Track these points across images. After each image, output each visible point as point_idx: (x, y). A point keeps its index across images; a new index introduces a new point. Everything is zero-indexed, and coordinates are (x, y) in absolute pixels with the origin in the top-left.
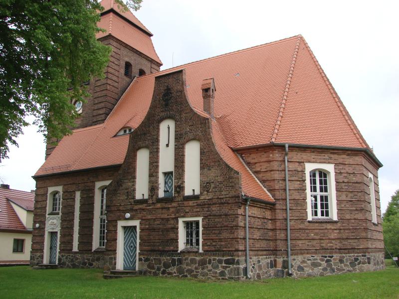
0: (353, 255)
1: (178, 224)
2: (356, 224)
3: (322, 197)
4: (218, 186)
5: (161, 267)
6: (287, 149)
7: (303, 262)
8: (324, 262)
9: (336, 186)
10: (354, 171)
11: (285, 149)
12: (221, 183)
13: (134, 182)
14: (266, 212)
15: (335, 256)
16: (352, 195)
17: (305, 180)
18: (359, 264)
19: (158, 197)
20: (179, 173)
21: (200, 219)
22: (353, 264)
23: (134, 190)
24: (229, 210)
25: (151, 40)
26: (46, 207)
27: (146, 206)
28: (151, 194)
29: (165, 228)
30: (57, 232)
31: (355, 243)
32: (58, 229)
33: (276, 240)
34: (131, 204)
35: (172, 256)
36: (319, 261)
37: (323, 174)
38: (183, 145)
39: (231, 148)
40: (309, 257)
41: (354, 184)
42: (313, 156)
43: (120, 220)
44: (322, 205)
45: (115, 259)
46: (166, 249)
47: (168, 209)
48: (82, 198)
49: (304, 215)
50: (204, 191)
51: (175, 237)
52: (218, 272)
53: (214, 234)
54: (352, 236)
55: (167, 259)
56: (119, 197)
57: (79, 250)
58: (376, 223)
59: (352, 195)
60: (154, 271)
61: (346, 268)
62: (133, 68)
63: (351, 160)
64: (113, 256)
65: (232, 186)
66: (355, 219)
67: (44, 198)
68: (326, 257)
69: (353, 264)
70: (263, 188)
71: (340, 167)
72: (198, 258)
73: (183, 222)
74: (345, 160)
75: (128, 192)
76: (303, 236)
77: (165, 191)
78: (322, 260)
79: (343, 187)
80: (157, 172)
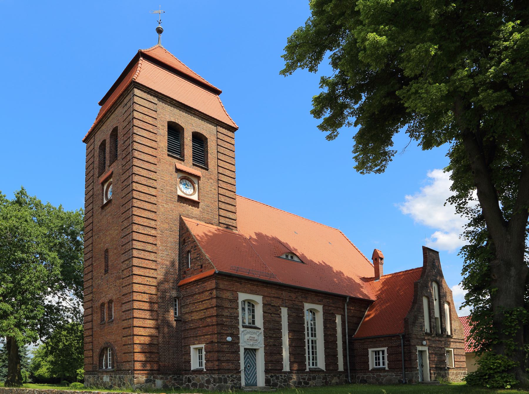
3: (312, 341)
21: (385, 349)
30: (426, 351)
34: (424, 335)
47: (441, 341)
48: (289, 316)
53: (459, 358)
57: (389, 369)
67: (234, 305)
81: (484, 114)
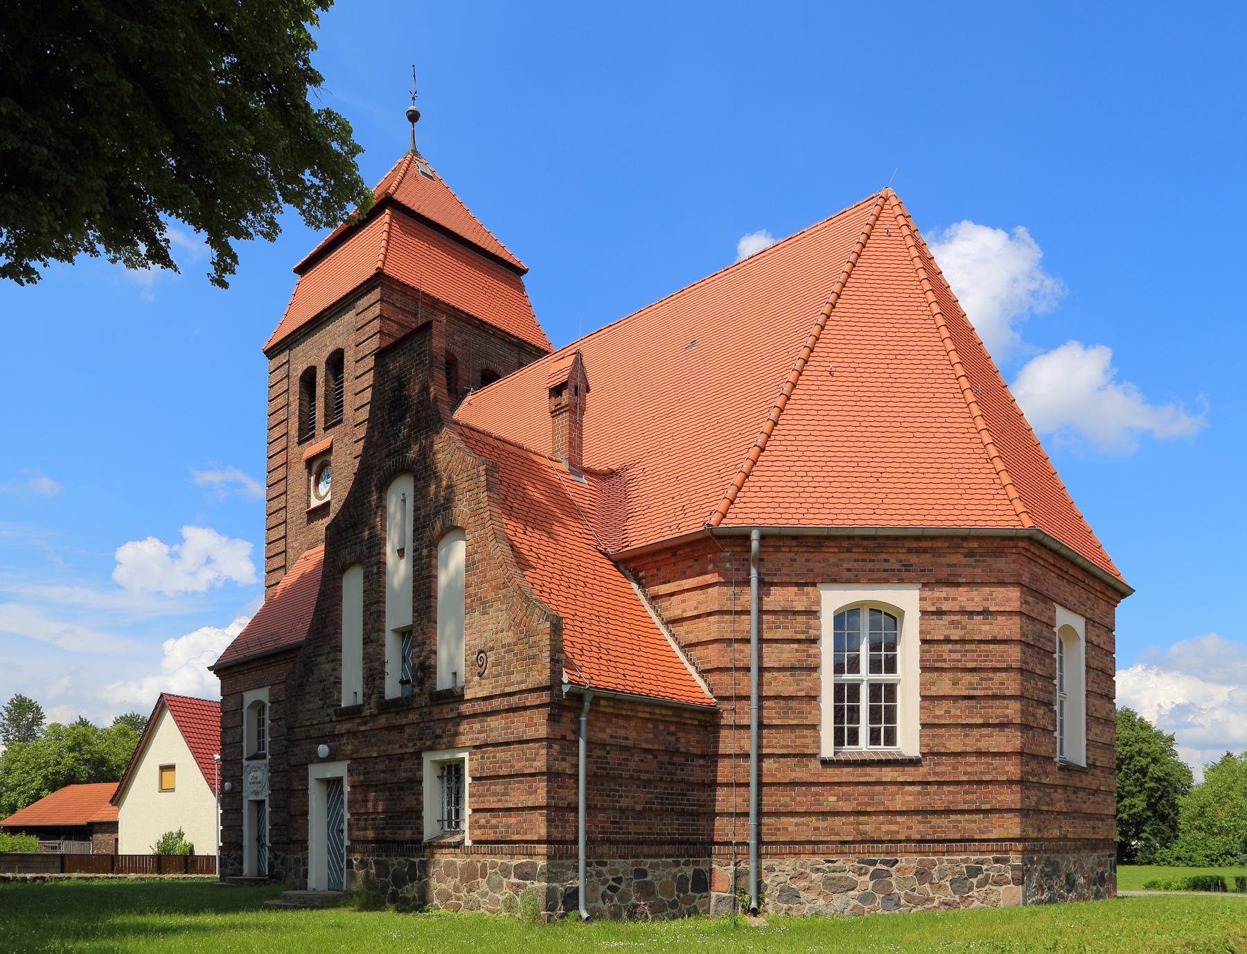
0: (961, 860)
2: (982, 768)
4: (503, 657)
5: (387, 885)
6: (755, 545)
8: (867, 878)
12: (509, 648)
13: (338, 661)
14: (681, 734)
15: (903, 861)
19: (383, 698)
22: (960, 884)
23: (338, 682)
26: (242, 741)
27: (358, 724)
28: (367, 691)
29: (396, 780)
31: (975, 822)
32: (265, 795)
34: (331, 721)
35: (409, 856)
36: (850, 875)
37: (894, 618)
38: (433, 545)
39: (606, 555)
41: (983, 647)
43: (312, 762)
45: (305, 861)
46: (398, 838)
47: (401, 728)
50: (472, 675)
51: (415, 803)
52: (501, 898)
53: (495, 794)
55: (399, 864)
56: (309, 702)
58: (1084, 764)
60: (375, 893)
61: (939, 897)
63: (978, 571)
64: (300, 856)
65: (534, 657)
66: (979, 754)
68: (873, 863)
69: (960, 884)
72: (459, 862)
73: (434, 762)
75: (323, 690)
76: (800, 804)
77: (403, 682)
79: (946, 656)
80: (383, 631)
81: (74, 70)
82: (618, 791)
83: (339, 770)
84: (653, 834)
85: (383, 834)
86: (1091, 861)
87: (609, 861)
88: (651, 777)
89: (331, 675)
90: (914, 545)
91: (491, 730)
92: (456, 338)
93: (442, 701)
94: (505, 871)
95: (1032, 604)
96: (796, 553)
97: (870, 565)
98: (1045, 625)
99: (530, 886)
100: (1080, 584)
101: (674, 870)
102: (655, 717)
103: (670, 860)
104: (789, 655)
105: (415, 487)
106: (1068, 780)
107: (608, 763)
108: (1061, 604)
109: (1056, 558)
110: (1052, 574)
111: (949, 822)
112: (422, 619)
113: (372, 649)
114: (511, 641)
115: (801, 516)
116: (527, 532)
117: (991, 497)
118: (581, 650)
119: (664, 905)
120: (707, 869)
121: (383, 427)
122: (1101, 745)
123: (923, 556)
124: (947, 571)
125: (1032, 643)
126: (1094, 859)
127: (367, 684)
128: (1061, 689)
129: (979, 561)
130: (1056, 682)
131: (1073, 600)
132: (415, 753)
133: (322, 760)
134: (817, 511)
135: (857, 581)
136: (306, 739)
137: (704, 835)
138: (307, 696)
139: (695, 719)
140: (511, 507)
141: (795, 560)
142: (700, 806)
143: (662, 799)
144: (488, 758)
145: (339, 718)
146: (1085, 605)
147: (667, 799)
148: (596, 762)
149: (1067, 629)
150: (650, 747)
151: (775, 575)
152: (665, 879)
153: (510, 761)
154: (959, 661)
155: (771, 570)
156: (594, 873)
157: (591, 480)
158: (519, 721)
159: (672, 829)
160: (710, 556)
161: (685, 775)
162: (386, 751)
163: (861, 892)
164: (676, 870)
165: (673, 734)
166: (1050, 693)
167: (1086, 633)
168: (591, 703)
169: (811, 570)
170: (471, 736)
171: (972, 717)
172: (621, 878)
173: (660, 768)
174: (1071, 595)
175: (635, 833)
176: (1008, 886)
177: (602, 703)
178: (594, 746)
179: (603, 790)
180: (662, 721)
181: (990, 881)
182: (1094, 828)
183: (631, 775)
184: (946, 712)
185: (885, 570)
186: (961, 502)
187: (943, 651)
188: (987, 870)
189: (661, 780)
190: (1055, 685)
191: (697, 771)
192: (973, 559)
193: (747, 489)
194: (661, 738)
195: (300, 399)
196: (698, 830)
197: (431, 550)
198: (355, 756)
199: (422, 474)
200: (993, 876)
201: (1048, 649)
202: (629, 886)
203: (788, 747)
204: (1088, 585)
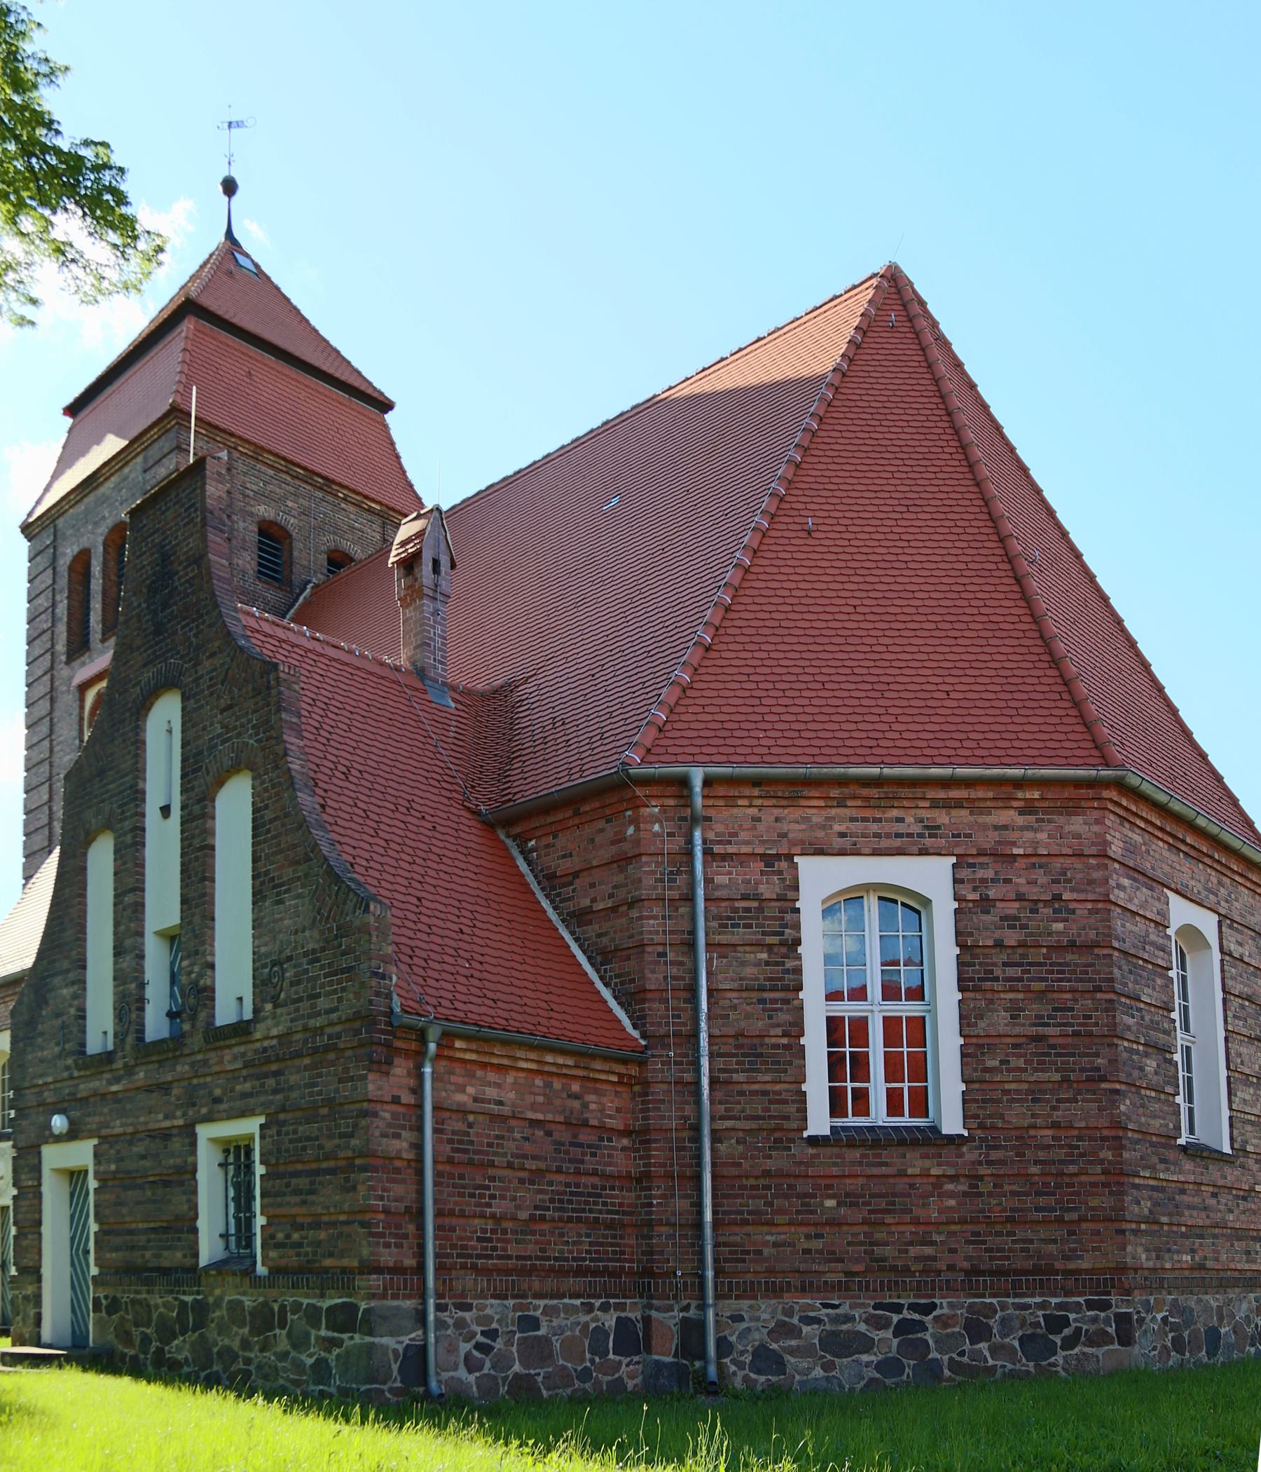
1: (193, 1152)
3: (891, 1024)
7: (783, 1330)
8: (888, 1334)
9: (961, 963)
10: (1056, 889)
11: (690, 796)
15: (944, 1305)
16: (1045, 1010)
17: (798, 942)
18: (1069, 1343)
20: (193, 931)
23: (82, 1016)
24: (340, 1081)
25: (386, 427)
33: (650, 1224)
34: (71, 1078)
35: (178, 1293)
36: (862, 1327)
40: (812, 1308)
42: (841, 820)
44: (861, 1066)
49: (792, 1108)
50: (264, 1001)
51: (186, 1207)
52: (310, 1361)
53: (297, 1192)
54: (1038, 1209)
59: (1045, 1010)
62: (298, 545)
63: (1042, 836)
65: (349, 969)
68: (897, 1308)
70: (599, 985)
71: (981, 874)
73: (214, 1140)
74: (1012, 836)
76: (781, 1211)
77: (171, 1015)
78: (880, 1324)
79: (998, 972)
80: (141, 934)
82: (488, 1188)
83: (81, 1154)
84: (548, 1259)
85: (143, 1256)
86: (1245, 1306)
87: (475, 1302)
88: (542, 1165)
89: (71, 1006)
90: (942, 794)
91: (291, 1088)
92: (290, 504)
93: (222, 1043)
94: (313, 1316)
95: (1128, 890)
96: (760, 807)
97: (874, 827)
98: (1152, 925)
99: (348, 1343)
100: (1206, 860)
101: (585, 1318)
102: (546, 1068)
103: (578, 1302)
104: (755, 970)
105: (183, 709)
106: (1202, 1174)
107: (472, 1143)
108: (1177, 892)
109: (1164, 818)
110: (1161, 844)
111: (1014, 1242)
112: (193, 915)
113: (128, 962)
114: (316, 946)
115: (766, 751)
116: (351, 778)
117: (1057, 720)
118: (425, 960)
119: (569, 1376)
120: (639, 1317)
121: (139, 621)
122: (1253, 1118)
123: (954, 812)
124: (994, 836)
125: (1132, 951)
126: (1250, 1303)
127: (121, 1020)
128: (1187, 1029)
129: (1042, 821)
130: (1175, 1015)
131: (1196, 887)
132: (185, 1126)
133: (59, 1139)
134: (789, 742)
135: (857, 853)
136: (39, 1106)
137: (631, 1261)
138: (40, 1040)
139: (613, 1073)
140: (328, 740)
141: (759, 820)
142: (624, 1213)
143: (561, 1201)
144: (287, 1134)
145: (82, 1073)
146: (1217, 896)
147: (570, 1202)
148: (450, 1141)
149: (1191, 933)
150: (540, 1117)
151: (729, 843)
152: (569, 1333)
153: (317, 1138)
154: (1020, 979)
155: (722, 834)
156: (450, 1321)
157: (461, 703)
158: (328, 1074)
159: (579, 1251)
160: (629, 813)
161: (598, 1163)
162: (146, 1123)
163: (880, 1357)
164: (586, 1318)
165: (576, 1097)
166: (1165, 1032)
167: (1221, 939)
168: (439, 1045)
169: (784, 835)
170: (262, 1099)
171: (1043, 1070)
172: (497, 1330)
173: (558, 1151)
174: (1192, 878)
175: (518, 1258)
176: (1111, 1347)
177: (458, 1044)
178: (447, 1114)
179: (464, 1187)
180: (558, 1075)
181: (1083, 1339)
182: (1248, 1253)
183: (508, 1162)
184: (1002, 1062)
185: (898, 835)
186: (1010, 728)
187: (995, 965)
188: (1075, 1320)
189: (559, 1171)
190: (1174, 1021)
191: (619, 1158)
192: (1033, 818)
193: (682, 709)
194: (557, 1102)
195: (68, 598)
196: (623, 1253)
197: (205, 807)
198: (104, 1132)
199: (191, 689)
200: (1087, 1331)
201: (1160, 962)
202: (509, 1343)
203: (757, 1118)
204: (1219, 862)
